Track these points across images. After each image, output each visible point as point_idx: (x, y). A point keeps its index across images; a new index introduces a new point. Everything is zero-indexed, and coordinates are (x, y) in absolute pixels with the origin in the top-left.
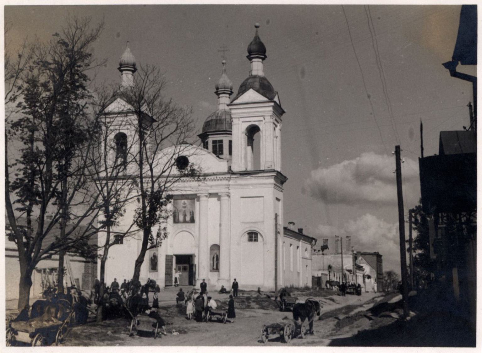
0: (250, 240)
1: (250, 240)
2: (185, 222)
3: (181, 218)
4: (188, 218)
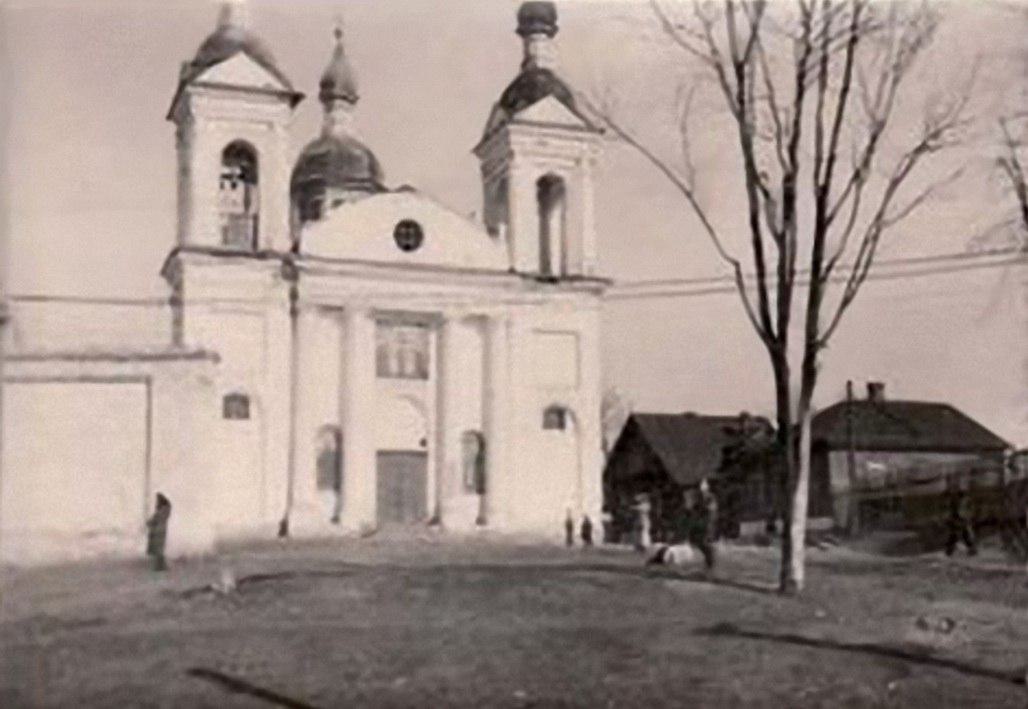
0: (547, 425)
1: (547, 425)
2: (401, 375)
3: (394, 366)
4: (410, 368)
